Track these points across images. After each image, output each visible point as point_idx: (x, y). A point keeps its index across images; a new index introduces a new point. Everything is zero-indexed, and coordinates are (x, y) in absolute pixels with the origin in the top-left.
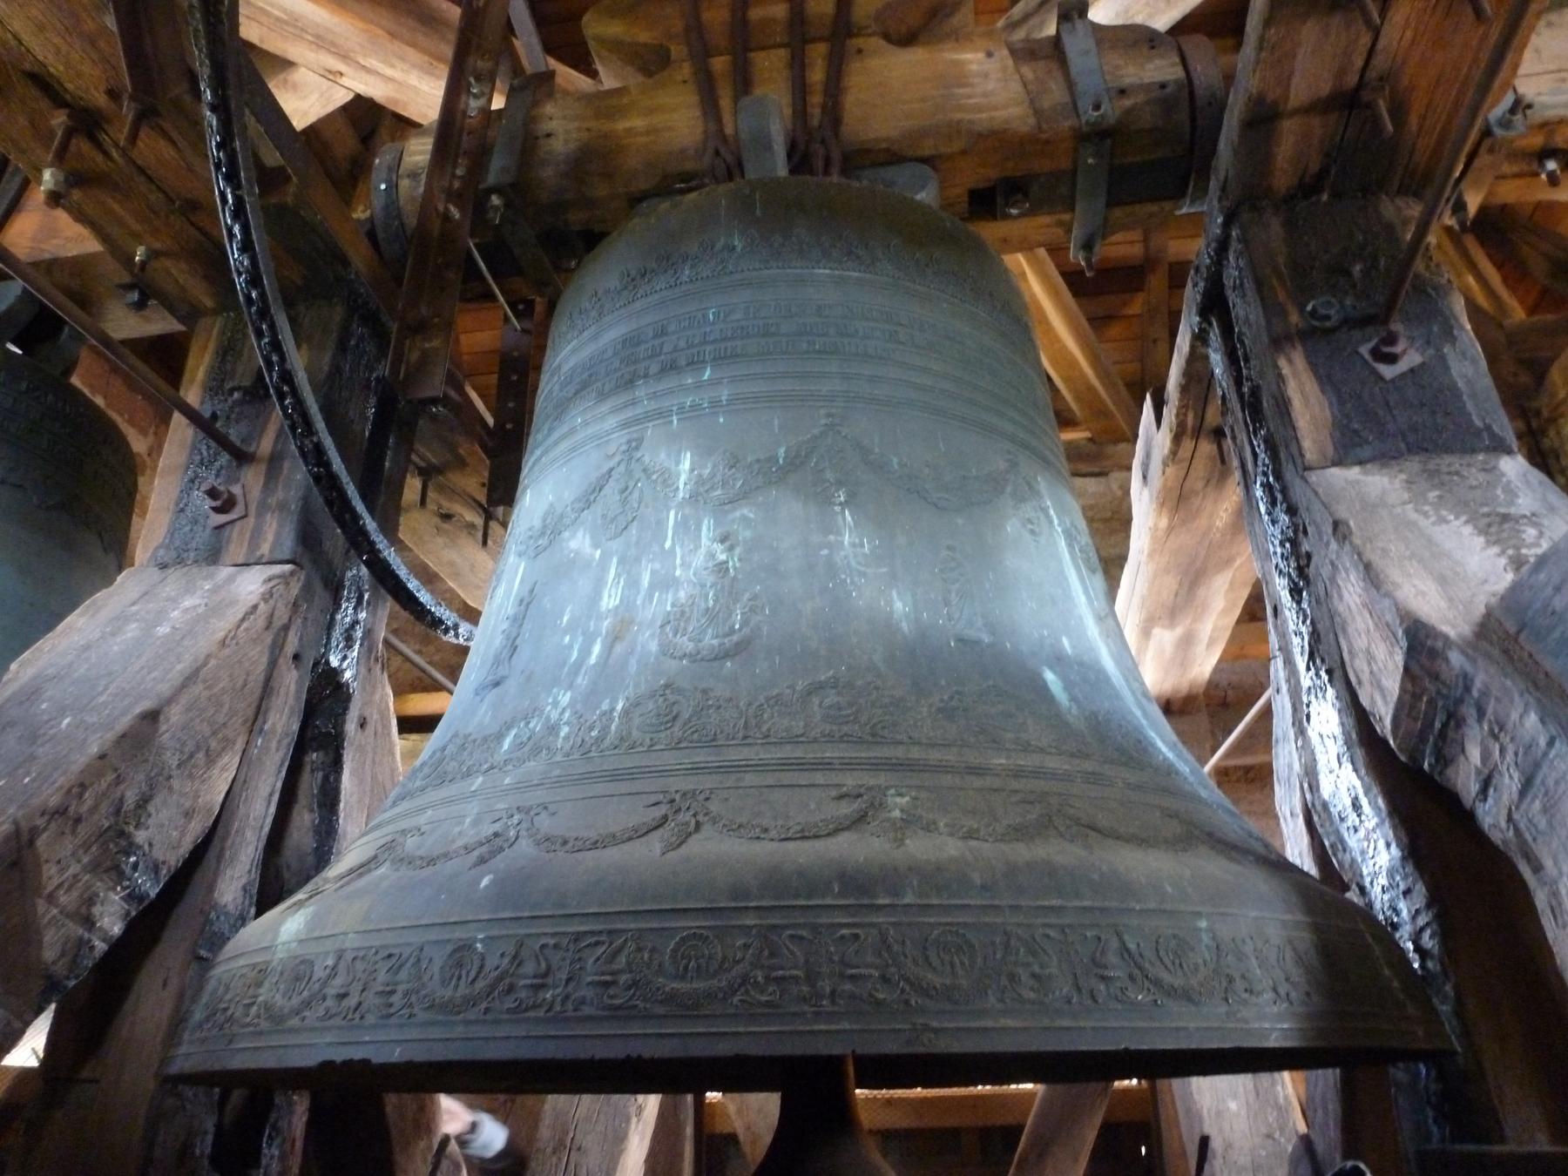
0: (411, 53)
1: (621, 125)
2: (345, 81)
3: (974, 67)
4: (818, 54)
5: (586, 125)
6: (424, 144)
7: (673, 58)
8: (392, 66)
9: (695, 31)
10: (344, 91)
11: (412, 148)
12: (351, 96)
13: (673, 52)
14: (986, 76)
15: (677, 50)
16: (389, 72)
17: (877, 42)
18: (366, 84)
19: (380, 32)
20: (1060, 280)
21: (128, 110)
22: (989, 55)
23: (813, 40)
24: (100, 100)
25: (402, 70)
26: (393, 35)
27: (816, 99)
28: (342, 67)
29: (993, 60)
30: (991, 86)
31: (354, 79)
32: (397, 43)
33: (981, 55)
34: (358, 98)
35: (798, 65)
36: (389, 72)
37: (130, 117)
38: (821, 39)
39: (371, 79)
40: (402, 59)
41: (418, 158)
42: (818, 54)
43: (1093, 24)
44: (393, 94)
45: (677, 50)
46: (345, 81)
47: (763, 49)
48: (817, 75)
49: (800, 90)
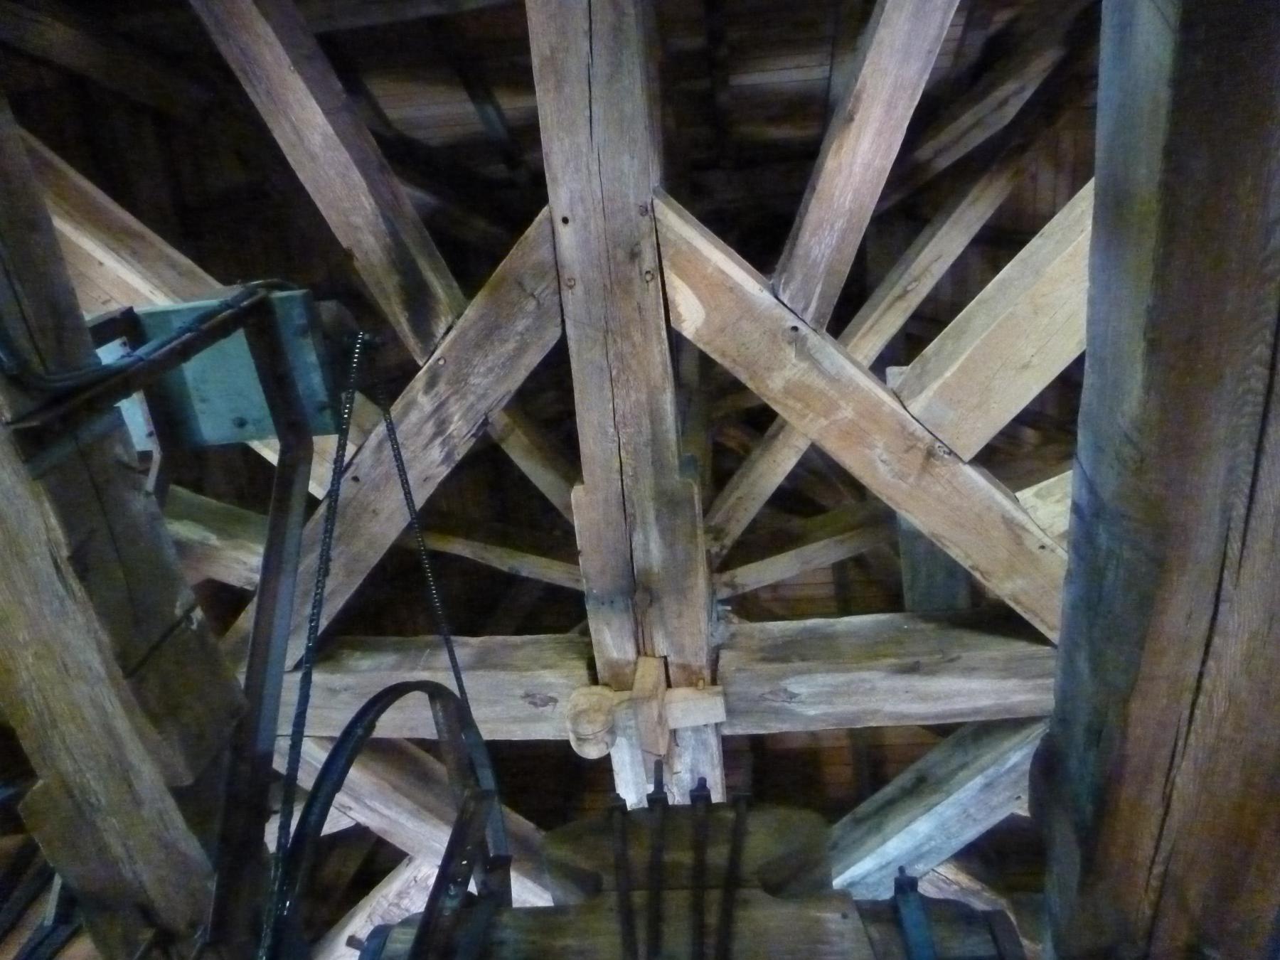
0: (407, 803)
1: (559, 943)
2: (352, 814)
3: (833, 926)
4: (714, 896)
5: (532, 938)
6: (404, 934)
7: (604, 886)
8: (390, 808)
9: (622, 865)
10: (349, 820)
11: (395, 935)
12: (353, 824)
13: (605, 882)
14: (841, 935)
15: (608, 880)
16: (386, 812)
17: (759, 894)
18: (367, 817)
19: (387, 785)
20: (949, 721)
21: (199, 937)
22: (845, 916)
23: (711, 887)
24: (181, 926)
25: (396, 812)
26: (396, 788)
27: (711, 941)
28: (353, 804)
29: (846, 921)
30: (847, 945)
31: (358, 813)
32: (397, 794)
33: (837, 916)
34: (358, 825)
35: (698, 909)
36: (386, 812)
37: (198, 945)
38: (716, 887)
39: (369, 814)
40: (398, 805)
41: (399, 946)
42: (714, 896)
43: (922, 897)
44: (386, 827)
45: (608, 880)
46: (352, 814)
47: (671, 889)
48: (712, 919)
49: (699, 930)
